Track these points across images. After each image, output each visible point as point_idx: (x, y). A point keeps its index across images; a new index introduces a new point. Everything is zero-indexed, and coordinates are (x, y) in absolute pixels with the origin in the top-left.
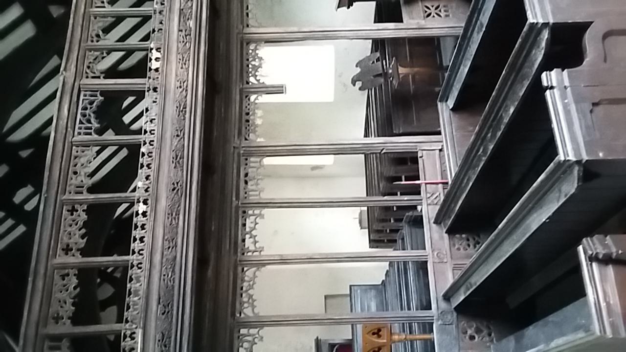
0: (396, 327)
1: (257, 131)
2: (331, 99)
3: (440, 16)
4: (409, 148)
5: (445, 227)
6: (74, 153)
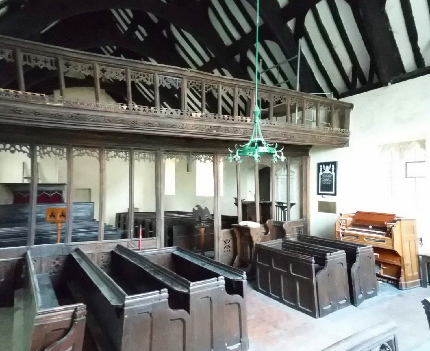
0: (64, 226)
3: (225, 248)
4: (158, 233)
5: (115, 250)
6: (150, 75)
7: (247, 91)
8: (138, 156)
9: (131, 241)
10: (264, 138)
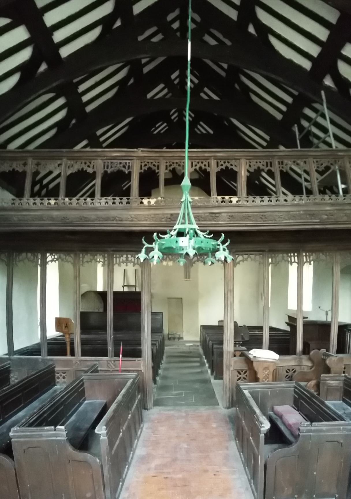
7: (206, 162)
8: (119, 260)
9: (111, 361)
10: (197, 224)
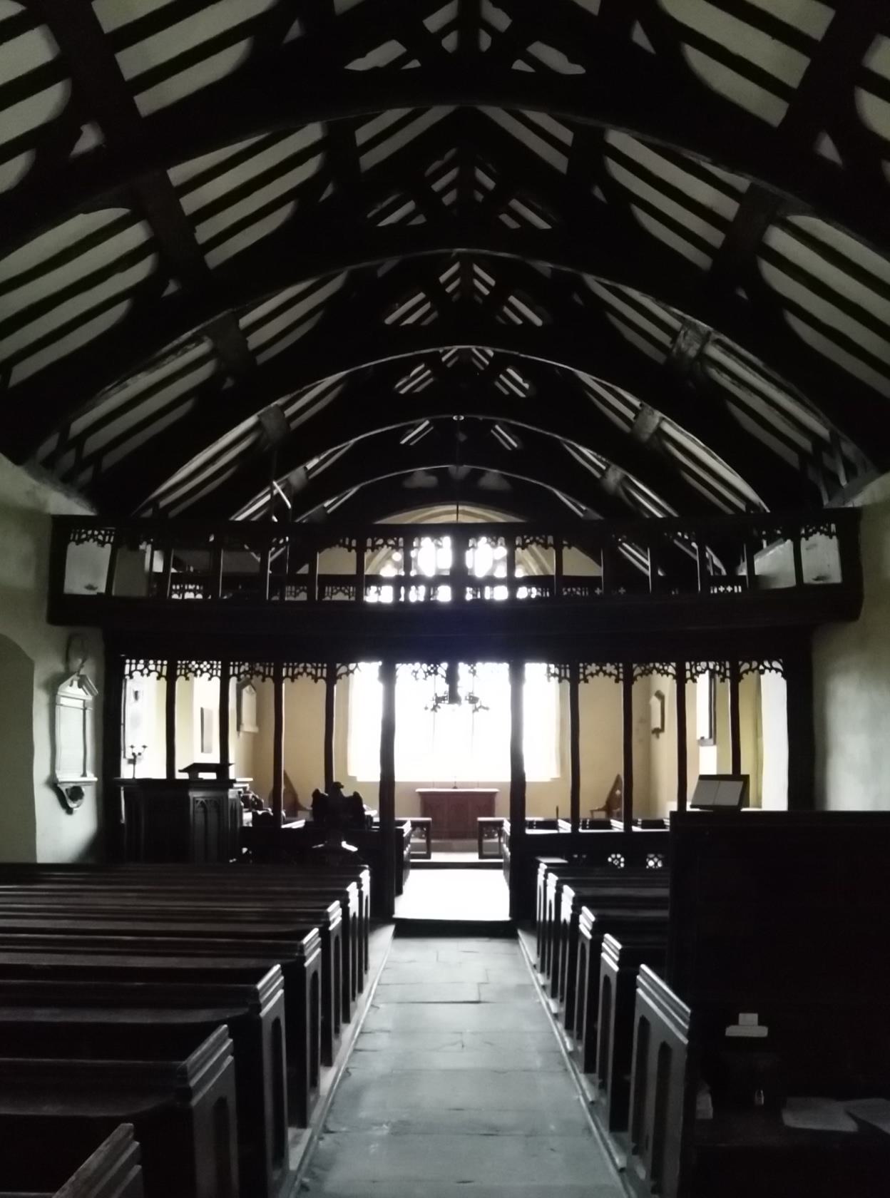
1: (591, 665)
2: (105, 32)
